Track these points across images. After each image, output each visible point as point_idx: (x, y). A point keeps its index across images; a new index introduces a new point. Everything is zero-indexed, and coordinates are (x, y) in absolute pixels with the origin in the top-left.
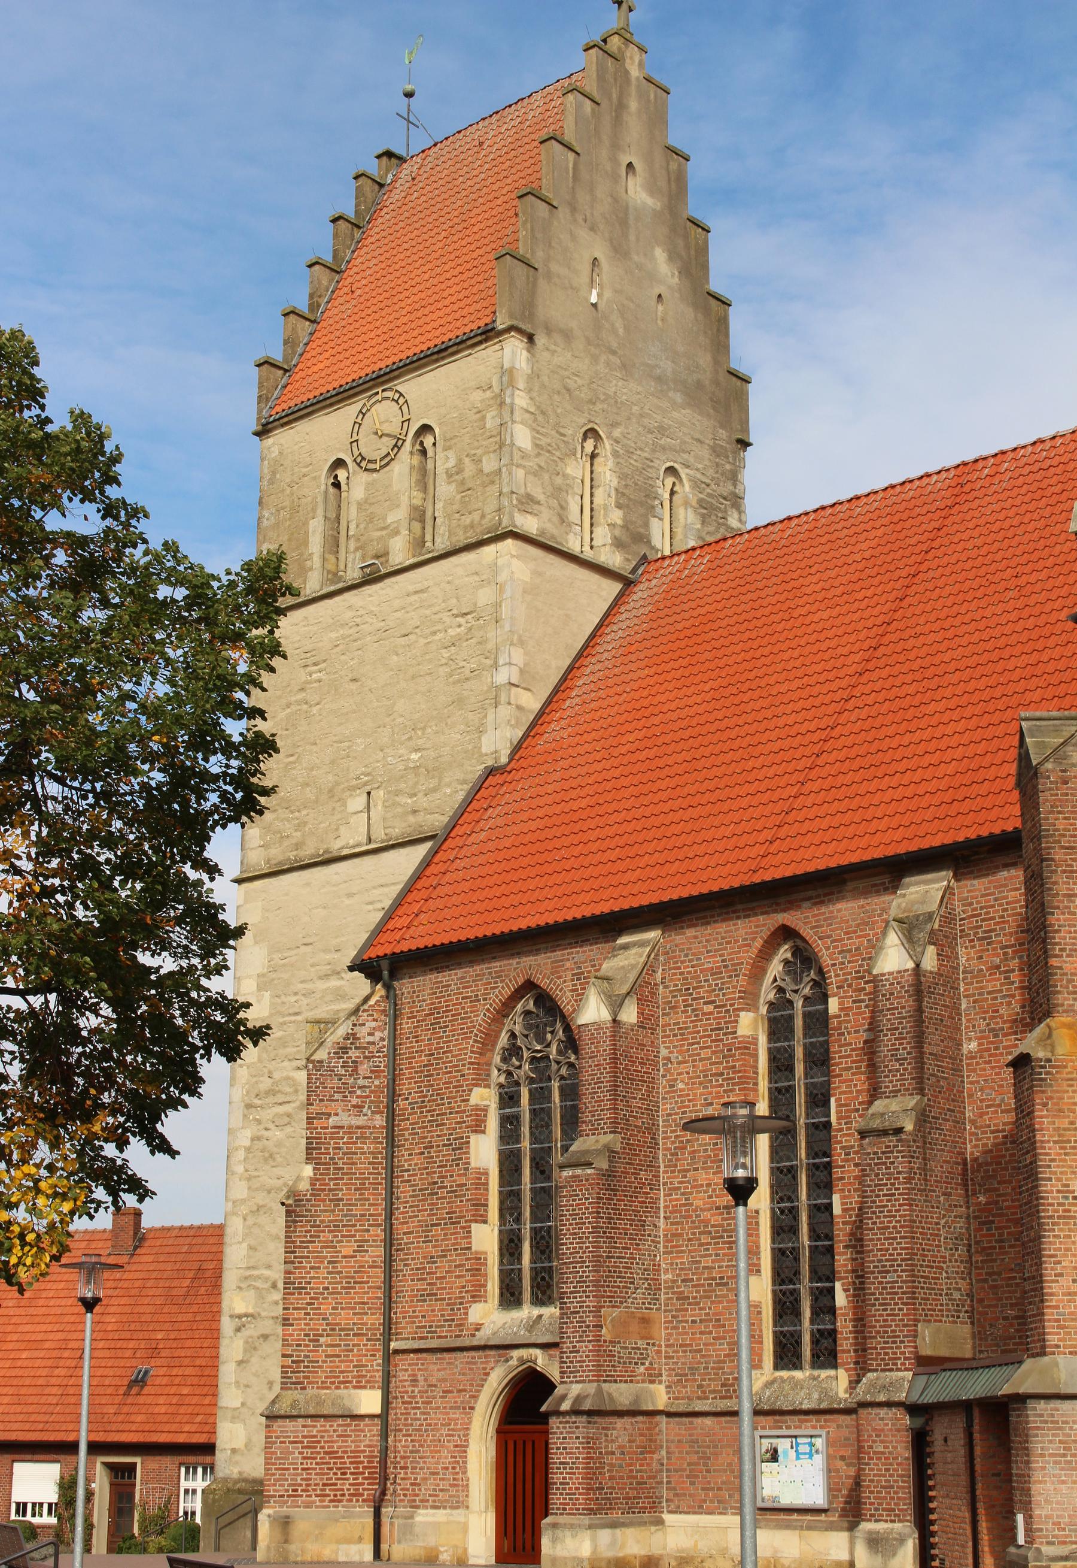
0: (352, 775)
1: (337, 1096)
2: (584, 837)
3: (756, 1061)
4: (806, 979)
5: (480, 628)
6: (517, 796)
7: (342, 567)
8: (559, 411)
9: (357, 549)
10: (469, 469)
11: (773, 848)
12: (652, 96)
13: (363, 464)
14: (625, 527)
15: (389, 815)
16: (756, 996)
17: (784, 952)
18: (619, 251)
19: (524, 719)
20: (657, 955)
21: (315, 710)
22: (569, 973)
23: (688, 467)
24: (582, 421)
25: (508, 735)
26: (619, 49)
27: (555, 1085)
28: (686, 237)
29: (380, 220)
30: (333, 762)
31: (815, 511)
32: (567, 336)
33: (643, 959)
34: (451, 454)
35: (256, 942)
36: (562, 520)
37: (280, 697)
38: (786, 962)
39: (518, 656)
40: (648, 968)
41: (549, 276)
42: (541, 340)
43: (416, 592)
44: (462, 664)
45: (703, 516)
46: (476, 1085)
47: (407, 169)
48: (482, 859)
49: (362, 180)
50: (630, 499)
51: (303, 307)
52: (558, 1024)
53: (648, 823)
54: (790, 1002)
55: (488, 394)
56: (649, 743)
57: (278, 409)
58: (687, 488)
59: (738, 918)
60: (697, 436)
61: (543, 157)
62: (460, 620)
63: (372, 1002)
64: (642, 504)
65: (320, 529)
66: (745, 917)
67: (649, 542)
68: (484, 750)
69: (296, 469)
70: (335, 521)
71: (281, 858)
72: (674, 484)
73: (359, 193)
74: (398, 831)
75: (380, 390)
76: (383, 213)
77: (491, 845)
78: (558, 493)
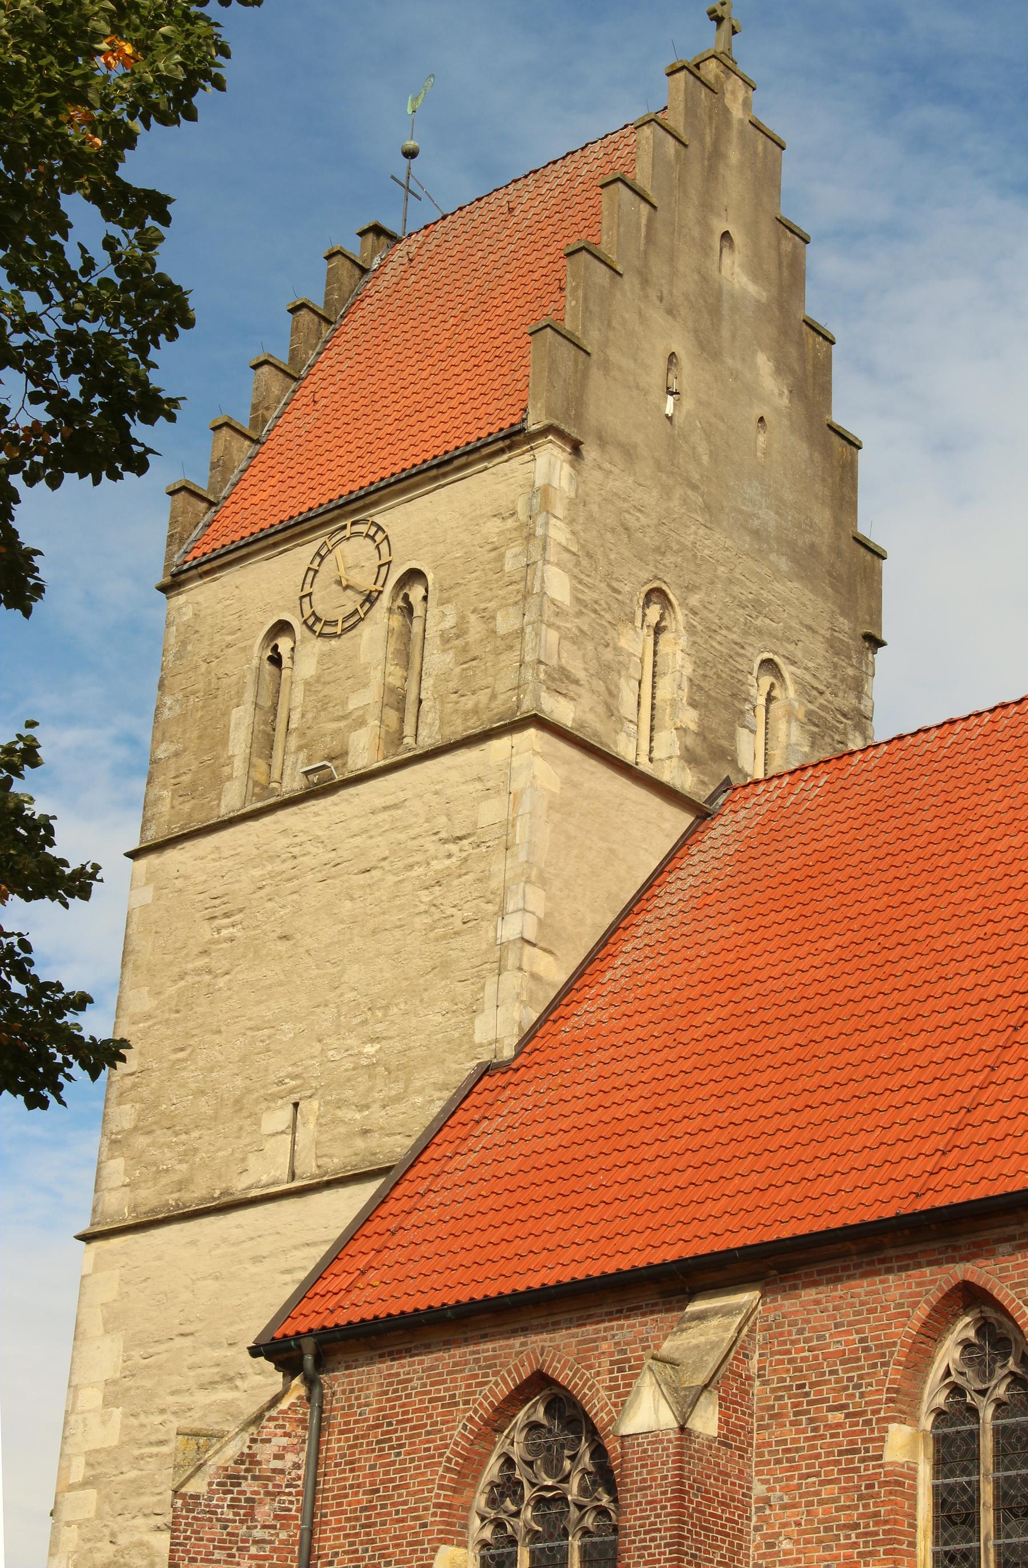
0: (272, 1078)
1: (218, 1555)
2: (635, 1156)
3: (914, 1506)
4: (1000, 1373)
5: (481, 858)
6: (527, 1102)
7: (276, 775)
8: (612, 556)
9: (300, 748)
10: (476, 628)
11: (949, 1161)
12: (760, 148)
13: (317, 627)
14: (701, 735)
15: (324, 1138)
16: (916, 1399)
17: (964, 1328)
18: (708, 348)
19: (541, 995)
20: (752, 1331)
21: (221, 982)
22: (606, 1361)
23: (794, 663)
24: (645, 575)
25: (516, 1016)
26: (717, 77)
27: (575, 1543)
28: (801, 344)
29: (360, 313)
30: (243, 1059)
31: (992, 711)
32: (629, 453)
33: (732, 1333)
34: (450, 609)
35: (107, 1332)
36: (611, 712)
37: (171, 964)
38: (967, 1345)
39: (536, 900)
40: (738, 1348)
41: (606, 366)
42: (590, 452)
43: (386, 808)
44: (450, 911)
45: (813, 736)
46: (445, 1541)
47: (400, 251)
48: (470, 1191)
49: (336, 261)
50: (709, 696)
51: (243, 419)
52: (584, 1445)
53: (739, 1133)
54: (973, 1411)
55: (510, 523)
56: (739, 1023)
57: (197, 553)
58: (791, 693)
59: (889, 1271)
60: (808, 621)
61: (604, 206)
62: (453, 848)
63: (284, 1405)
64: (726, 706)
65: (248, 720)
66: (901, 1269)
67: (734, 762)
68: (478, 1039)
69: (217, 637)
70: (269, 713)
71: (154, 1203)
72: (772, 686)
73: (332, 276)
74: (336, 1163)
75: (349, 522)
76: (364, 305)
77: (485, 1172)
78: (607, 672)
